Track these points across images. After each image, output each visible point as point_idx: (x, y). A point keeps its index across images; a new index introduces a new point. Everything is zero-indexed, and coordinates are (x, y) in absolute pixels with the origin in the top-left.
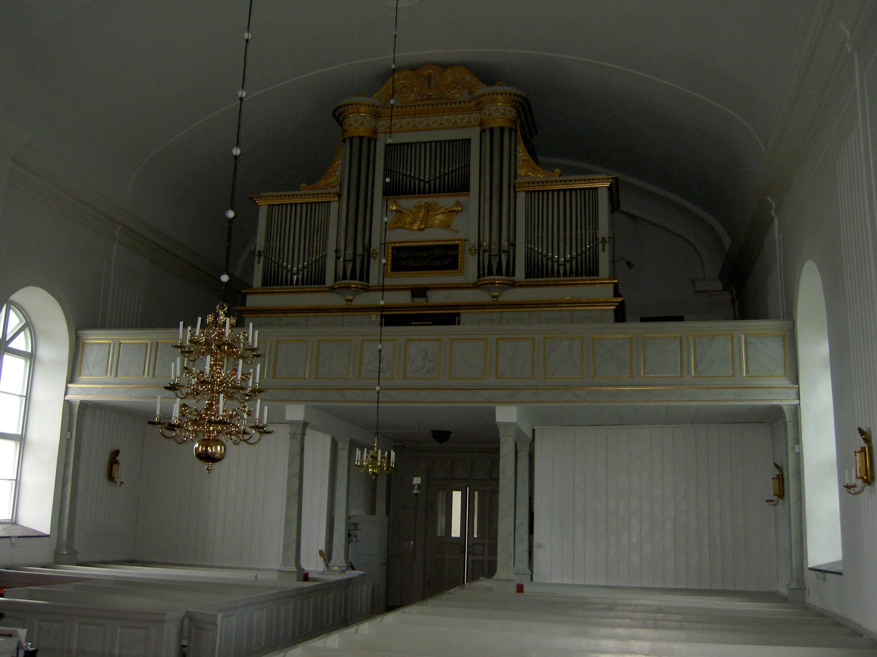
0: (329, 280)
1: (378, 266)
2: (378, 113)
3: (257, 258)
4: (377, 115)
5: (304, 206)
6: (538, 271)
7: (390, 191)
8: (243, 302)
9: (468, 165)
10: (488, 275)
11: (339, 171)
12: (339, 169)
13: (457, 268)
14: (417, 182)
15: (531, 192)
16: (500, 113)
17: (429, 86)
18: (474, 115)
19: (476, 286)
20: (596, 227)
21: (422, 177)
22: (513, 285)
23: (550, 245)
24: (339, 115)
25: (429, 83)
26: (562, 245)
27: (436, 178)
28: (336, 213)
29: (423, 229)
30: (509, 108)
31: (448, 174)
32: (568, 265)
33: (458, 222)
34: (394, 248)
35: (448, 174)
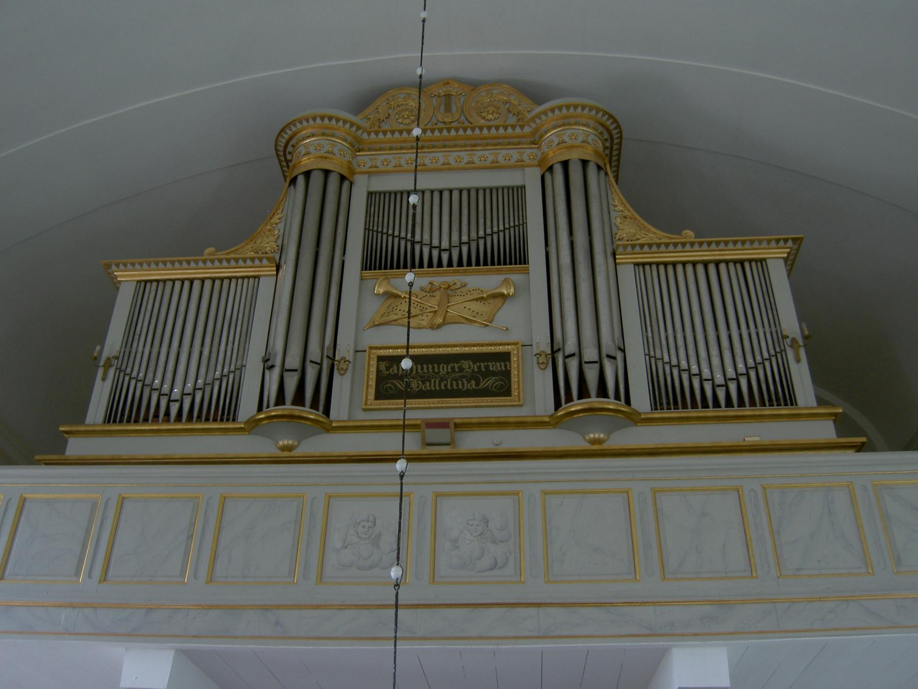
0: (247, 407)
1: (349, 394)
2: (359, 141)
3: (100, 372)
4: (357, 146)
5: (208, 284)
6: (672, 397)
7: (377, 260)
8: (62, 450)
9: (522, 225)
10: (580, 397)
11: (287, 218)
12: (281, 226)
13: (508, 393)
14: (426, 251)
15: (644, 264)
16: (581, 141)
17: (448, 109)
18: (528, 151)
19: (553, 423)
20: (775, 321)
21: (435, 242)
22: (635, 419)
23: (692, 352)
24: (284, 153)
25: (447, 106)
26: (714, 351)
27: (461, 243)
28: (272, 293)
29: (439, 326)
30: (592, 137)
31: (498, 233)
32: (733, 387)
33: (507, 315)
34: (380, 359)
35: (498, 233)
